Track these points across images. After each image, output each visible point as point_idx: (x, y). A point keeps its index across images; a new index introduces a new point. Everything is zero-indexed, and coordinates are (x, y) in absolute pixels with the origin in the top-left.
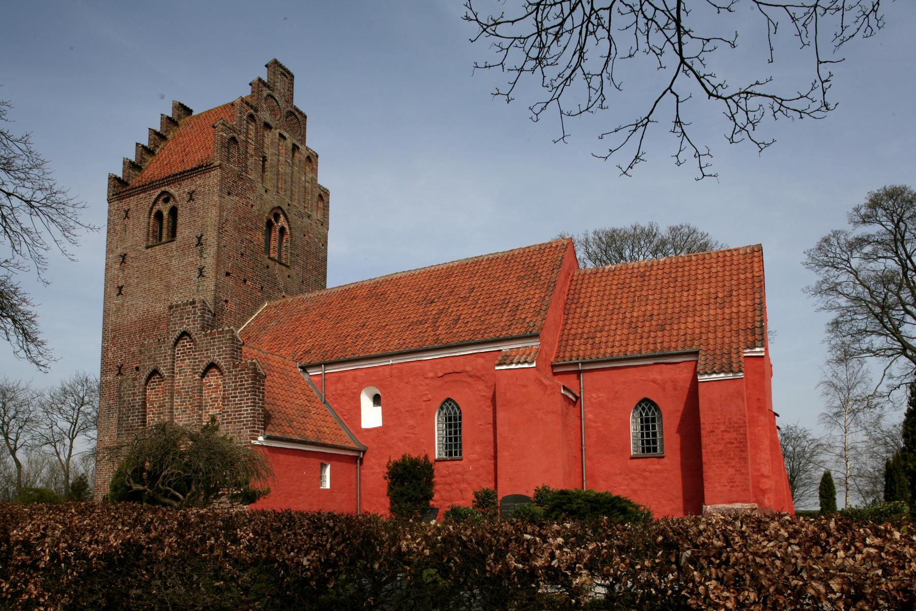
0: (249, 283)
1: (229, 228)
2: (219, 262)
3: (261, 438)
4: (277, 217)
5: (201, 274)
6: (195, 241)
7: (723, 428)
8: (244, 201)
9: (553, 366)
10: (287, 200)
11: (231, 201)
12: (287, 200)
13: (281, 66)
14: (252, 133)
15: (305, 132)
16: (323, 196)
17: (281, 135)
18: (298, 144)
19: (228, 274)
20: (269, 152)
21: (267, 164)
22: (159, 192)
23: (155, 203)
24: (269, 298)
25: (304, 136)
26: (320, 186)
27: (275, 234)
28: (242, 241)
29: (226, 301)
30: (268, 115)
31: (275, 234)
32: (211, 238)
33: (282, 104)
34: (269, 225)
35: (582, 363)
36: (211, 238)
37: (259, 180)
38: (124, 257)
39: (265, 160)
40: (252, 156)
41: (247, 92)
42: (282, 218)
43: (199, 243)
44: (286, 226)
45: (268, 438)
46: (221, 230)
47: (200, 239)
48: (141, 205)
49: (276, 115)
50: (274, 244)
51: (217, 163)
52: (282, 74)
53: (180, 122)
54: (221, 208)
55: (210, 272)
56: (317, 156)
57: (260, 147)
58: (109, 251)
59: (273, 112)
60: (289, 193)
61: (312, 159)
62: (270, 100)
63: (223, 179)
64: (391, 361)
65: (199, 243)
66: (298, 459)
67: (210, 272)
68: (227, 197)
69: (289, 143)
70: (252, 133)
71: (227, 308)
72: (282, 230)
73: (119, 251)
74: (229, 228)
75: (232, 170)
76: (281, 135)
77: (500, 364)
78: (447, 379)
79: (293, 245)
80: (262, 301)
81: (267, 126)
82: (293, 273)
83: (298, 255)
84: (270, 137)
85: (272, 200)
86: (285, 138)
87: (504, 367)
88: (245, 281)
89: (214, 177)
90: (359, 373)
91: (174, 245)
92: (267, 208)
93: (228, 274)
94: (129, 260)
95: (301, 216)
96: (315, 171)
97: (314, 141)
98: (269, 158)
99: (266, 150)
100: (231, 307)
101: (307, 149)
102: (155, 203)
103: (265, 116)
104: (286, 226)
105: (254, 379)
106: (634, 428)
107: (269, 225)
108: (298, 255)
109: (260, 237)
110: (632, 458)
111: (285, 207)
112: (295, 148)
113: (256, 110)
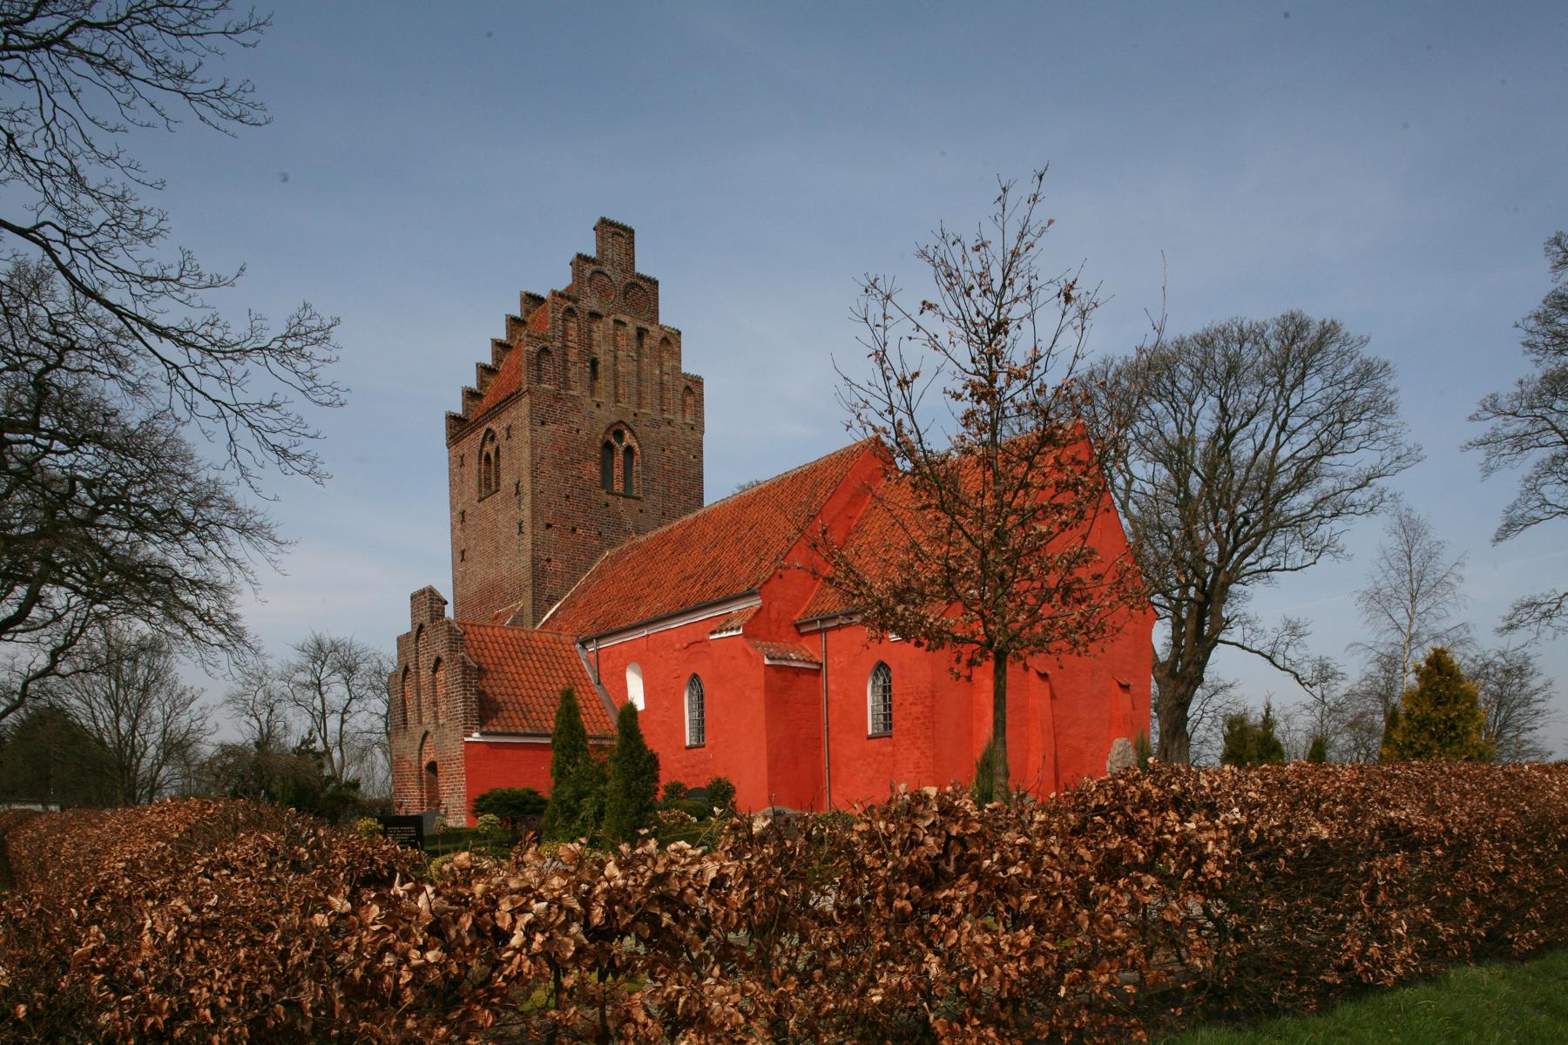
0: (580, 531)
1: (547, 467)
2: (535, 513)
3: (476, 735)
4: (619, 435)
5: (521, 532)
6: (514, 489)
7: (911, 699)
8: (565, 427)
9: (797, 627)
10: (633, 409)
11: (545, 433)
12: (633, 409)
13: (612, 224)
14: (573, 334)
15: (656, 304)
16: (693, 387)
17: (617, 322)
18: (647, 326)
19: (549, 526)
20: (602, 352)
21: (600, 368)
22: (483, 431)
23: (483, 444)
24: (612, 545)
25: (655, 312)
26: (685, 376)
27: (619, 458)
28: (566, 480)
29: (549, 560)
30: (594, 301)
31: (619, 458)
32: (526, 487)
33: (617, 277)
34: (608, 447)
35: (822, 621)
36: (526, 487)
37: (587, 394)
38: (463, 513)
39: (594, 363)
40: (575, 364)
41: (562, 279)
42: (627, 434)
43: (518, 493)
44: (635, 444)
45: (482, 734)
46: (535, 472)
47: (517, 486)
48: (472, 443)
49: (608, 296)
50: (618, 472)
51: (525, 388)
52: (614, 234)
53: (529, 320)
54: (534, 445)
55: (527, 528)
56: (679, 333)
57: (587, 344)
58: (453, 508)
59: (603, 293)
60: (635, 398)
61: (671, 340)
62: (598, 277)
63: (532, 406)
64: (628, 637)
65: (518, 493)
66: (530, 753)
67: (527, 528)
68: (540, 429)
69: (631, 329)
70: (573, 334)
71: (550, 568)
72: (629, 450)
73: (459, 508)
74: (547, 467)
75: (546, 391)
76: (617, 322)
77: (713, 633)
78: (693, 649)
79: (646, 467)
80: (602, 550)
81: (595, 316)
82: (647, 505)
83: (653, 480)
84: (600, 330)
85: (607, 415)
86: (624, 324)
87: (724, 635)
88: (574, 530)
89: (523, 408)
90: (624, 647)
91: (498, 496)
92: (601, 428)
93: (549, 526)
94: (467, 518)
95: (656, 424)
96: (677, 356)
97: (669, 315)
98: (601, 359)
99: (596, 349)
100: (557, 565)
101: (662, 328)
102: (483, 444)
103: (591, 303)
104: (635, 444)
105: (464, 672)
106: (871, 701)
107: (608, 447)
108: (653, 480)
109: (593, 469)
110: (869, 738)
111: (629, 420)
112: (641, 333)
113: (576, 301)
